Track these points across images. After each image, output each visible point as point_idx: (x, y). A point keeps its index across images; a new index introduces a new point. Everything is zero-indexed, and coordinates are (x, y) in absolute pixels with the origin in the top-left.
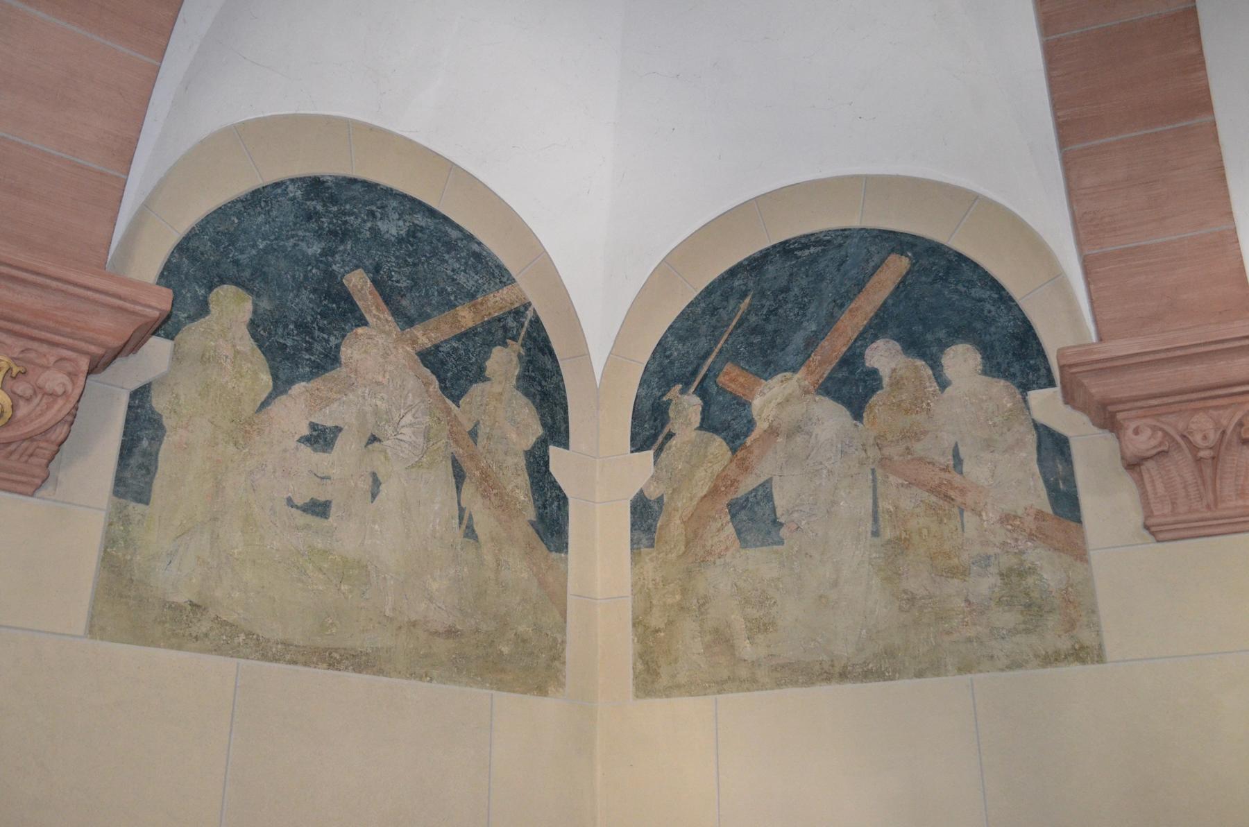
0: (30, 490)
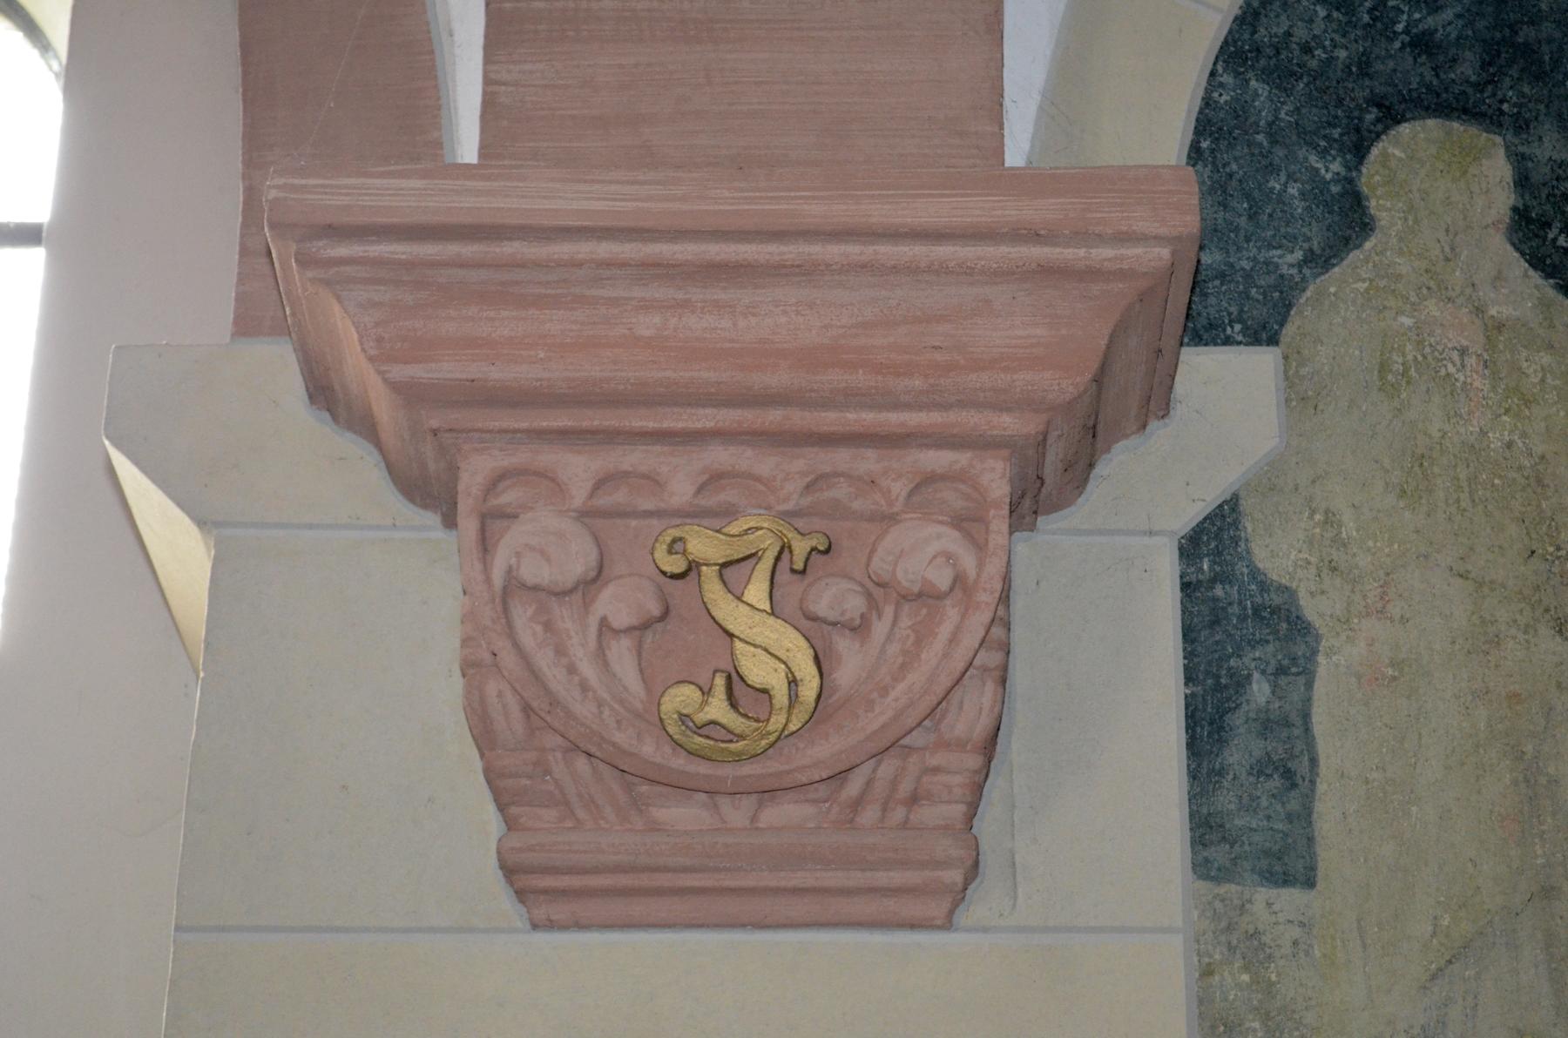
0: (937, 909)
